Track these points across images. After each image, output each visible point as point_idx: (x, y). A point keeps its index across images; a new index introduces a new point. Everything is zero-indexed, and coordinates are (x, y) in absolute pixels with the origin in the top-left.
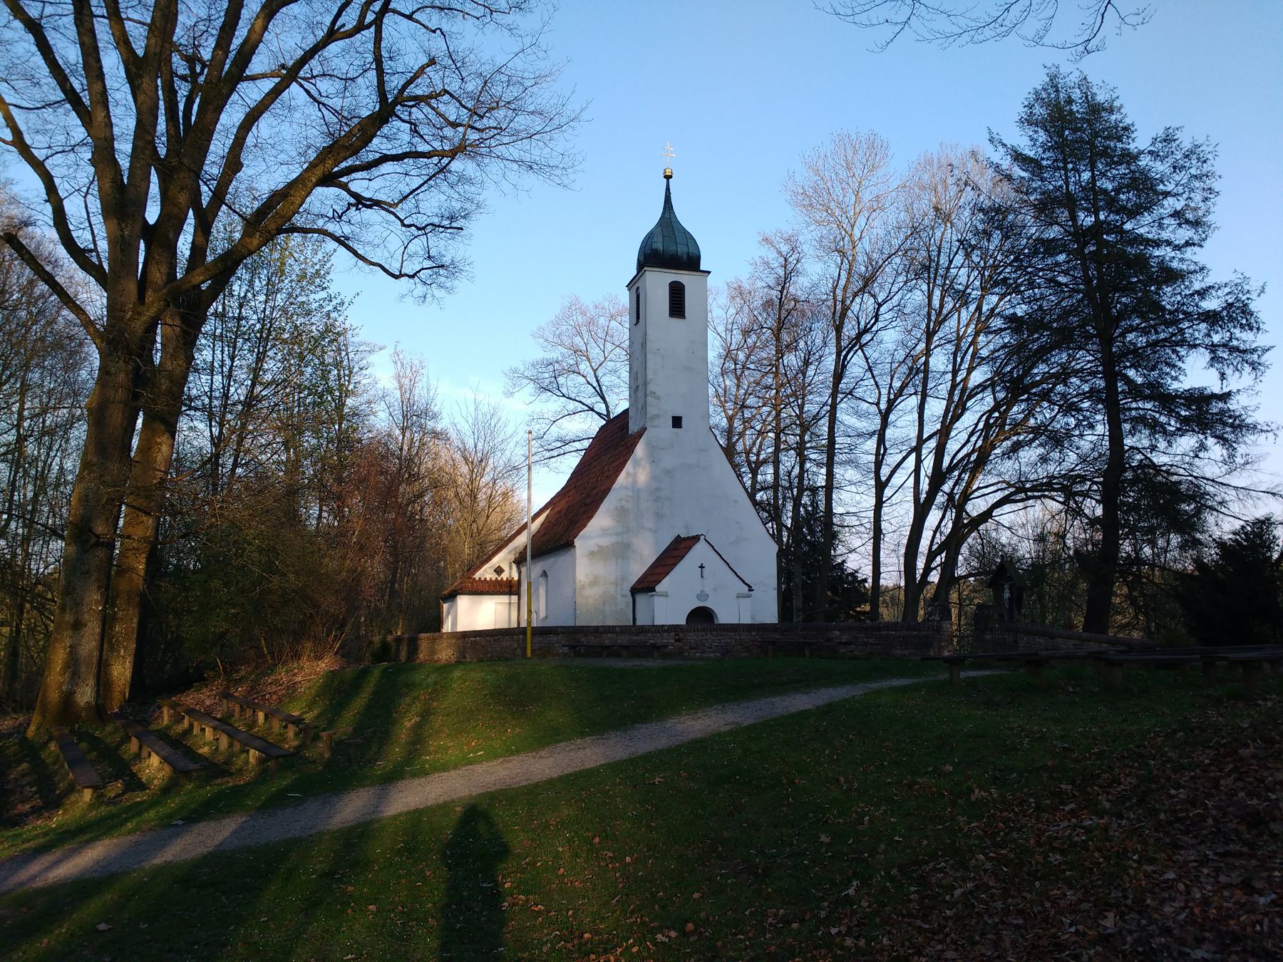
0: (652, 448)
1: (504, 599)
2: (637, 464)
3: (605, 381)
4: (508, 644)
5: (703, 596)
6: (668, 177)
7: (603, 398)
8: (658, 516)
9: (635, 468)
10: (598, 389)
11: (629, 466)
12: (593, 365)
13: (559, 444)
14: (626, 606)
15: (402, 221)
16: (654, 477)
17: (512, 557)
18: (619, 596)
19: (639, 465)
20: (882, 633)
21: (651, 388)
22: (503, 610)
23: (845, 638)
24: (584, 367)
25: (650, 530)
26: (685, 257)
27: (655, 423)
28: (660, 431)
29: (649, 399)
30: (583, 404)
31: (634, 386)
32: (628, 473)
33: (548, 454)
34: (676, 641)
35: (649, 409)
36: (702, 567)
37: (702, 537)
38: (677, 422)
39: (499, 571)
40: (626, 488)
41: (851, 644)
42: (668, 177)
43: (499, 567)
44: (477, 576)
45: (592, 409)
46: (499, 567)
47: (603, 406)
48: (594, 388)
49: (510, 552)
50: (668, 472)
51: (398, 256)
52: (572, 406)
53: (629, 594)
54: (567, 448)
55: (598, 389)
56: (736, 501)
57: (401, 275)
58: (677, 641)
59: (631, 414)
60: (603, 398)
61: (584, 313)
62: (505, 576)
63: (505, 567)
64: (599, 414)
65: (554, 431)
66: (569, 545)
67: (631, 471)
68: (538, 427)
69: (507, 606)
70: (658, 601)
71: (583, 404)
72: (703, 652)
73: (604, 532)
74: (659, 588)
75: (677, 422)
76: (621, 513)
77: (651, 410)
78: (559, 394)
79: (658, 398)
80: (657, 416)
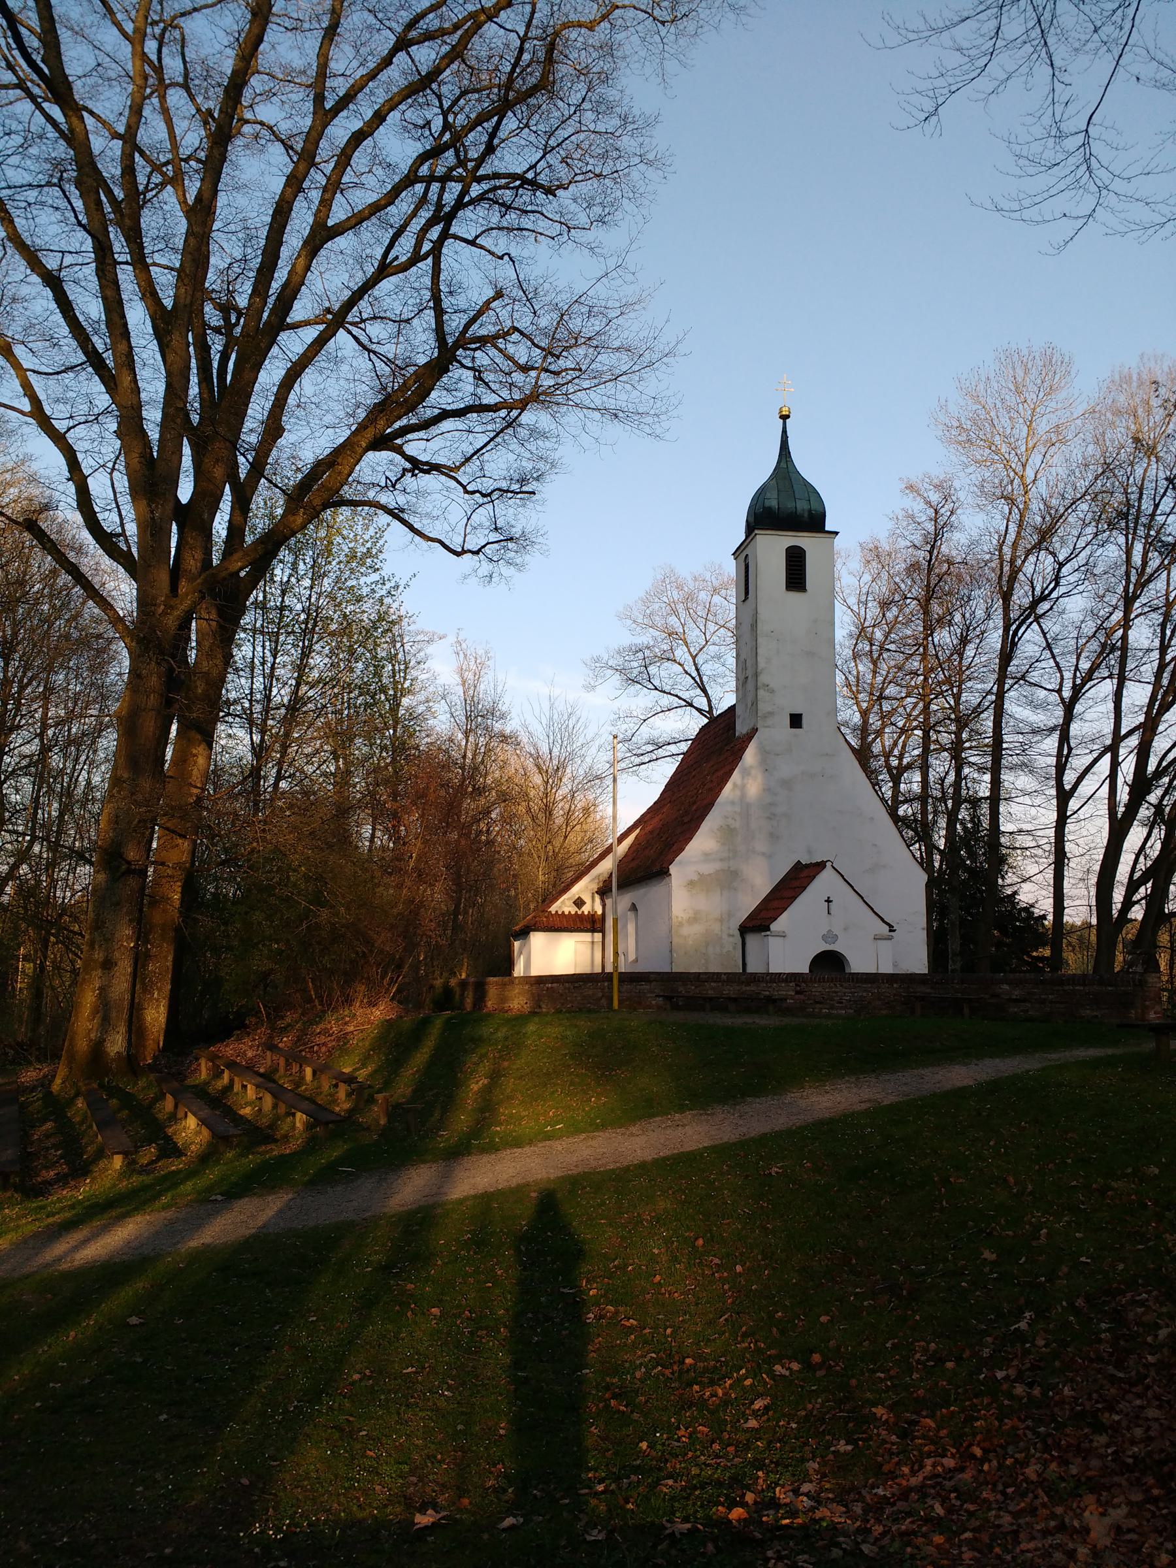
0: (764, 753)
1: (586, 937)
2: (746, 773)
3: (706, 669)
4: (590, 993)
5: (830, 937)
6: (785, 418)
7: (704, 690)
8: (774, 837)
9: (743, 778)
10: (698, 679)
11: (736, 776)
12: (692, 650)
13: (650, 748)
14: (734, 948)
15: (464, 487)
16: (767, 790)
17: (595, 887)
18: (725, 936)
19: (749, 774)
20: (1066, 988)
21: (763, 679)
22: (585, 950)
23: (1017, 993)
24: (681, 653)
25: (763, 854)
26: (806, 515)
27: (769, 722)
28: (775, 731)
29: (761, 693)
30: (680, 698)
31: (742, 678)
32: (735, 785)
33: (637, 760)
34: (797, 993)
35: (761, 706)
36: (828, 901)
37: (829, 864)
38: (796, 721)
39: (579, 903)
40: (733, 803)
41: (1024, 1001)
42: (785, 418)
43: (579, 898)
44: (553, 909)
45: (691, 705)
46: (579, 898)
47: (705, 700)
48: (693, 678)
49: (593, 880)
50: (786, 784)
51: (460, 529)
52: (666, 700)
53: (737, 933)
54: (661, 752)
55: (698, 679)
56: (872, 819)
57: (464, 552)
58: (797, 993)
59: (738, 711)
60: (704, 690)
61: (680, 588)
62: (586, 909)
63: (587, 898)
64: (699, 710)
65: (645, 732)
66: (664, 873)
67: (739, 782)
68: (625, 726)
69: (589, 946)
70: (773, 942)
71: (680, 698)
72: (832, 1007)
73: (707, 856)
74: (774, 927)
75: (796, 721)
76: (727, 834)
77: (763, 707)
78: (650, 686)
79: (772, 691)
80: (771, 714)
